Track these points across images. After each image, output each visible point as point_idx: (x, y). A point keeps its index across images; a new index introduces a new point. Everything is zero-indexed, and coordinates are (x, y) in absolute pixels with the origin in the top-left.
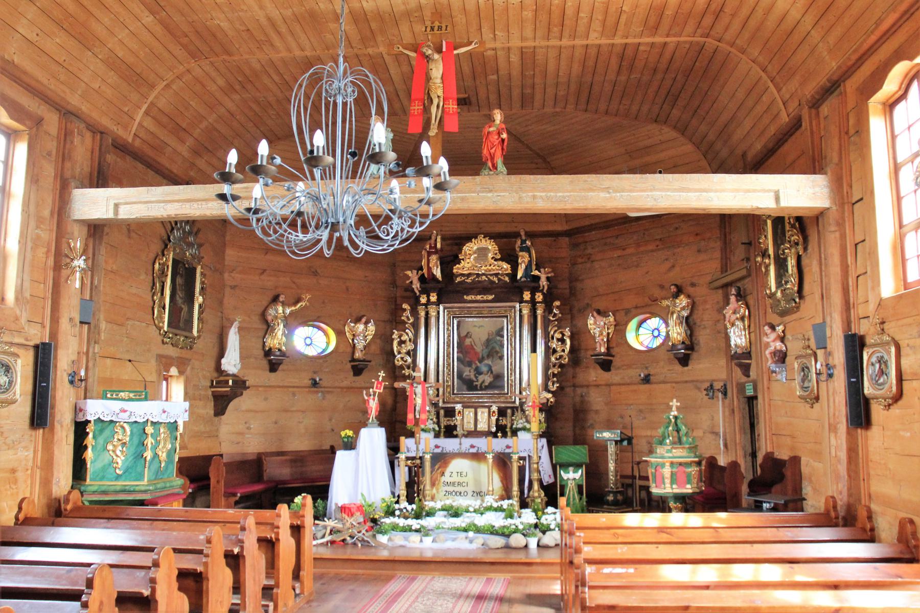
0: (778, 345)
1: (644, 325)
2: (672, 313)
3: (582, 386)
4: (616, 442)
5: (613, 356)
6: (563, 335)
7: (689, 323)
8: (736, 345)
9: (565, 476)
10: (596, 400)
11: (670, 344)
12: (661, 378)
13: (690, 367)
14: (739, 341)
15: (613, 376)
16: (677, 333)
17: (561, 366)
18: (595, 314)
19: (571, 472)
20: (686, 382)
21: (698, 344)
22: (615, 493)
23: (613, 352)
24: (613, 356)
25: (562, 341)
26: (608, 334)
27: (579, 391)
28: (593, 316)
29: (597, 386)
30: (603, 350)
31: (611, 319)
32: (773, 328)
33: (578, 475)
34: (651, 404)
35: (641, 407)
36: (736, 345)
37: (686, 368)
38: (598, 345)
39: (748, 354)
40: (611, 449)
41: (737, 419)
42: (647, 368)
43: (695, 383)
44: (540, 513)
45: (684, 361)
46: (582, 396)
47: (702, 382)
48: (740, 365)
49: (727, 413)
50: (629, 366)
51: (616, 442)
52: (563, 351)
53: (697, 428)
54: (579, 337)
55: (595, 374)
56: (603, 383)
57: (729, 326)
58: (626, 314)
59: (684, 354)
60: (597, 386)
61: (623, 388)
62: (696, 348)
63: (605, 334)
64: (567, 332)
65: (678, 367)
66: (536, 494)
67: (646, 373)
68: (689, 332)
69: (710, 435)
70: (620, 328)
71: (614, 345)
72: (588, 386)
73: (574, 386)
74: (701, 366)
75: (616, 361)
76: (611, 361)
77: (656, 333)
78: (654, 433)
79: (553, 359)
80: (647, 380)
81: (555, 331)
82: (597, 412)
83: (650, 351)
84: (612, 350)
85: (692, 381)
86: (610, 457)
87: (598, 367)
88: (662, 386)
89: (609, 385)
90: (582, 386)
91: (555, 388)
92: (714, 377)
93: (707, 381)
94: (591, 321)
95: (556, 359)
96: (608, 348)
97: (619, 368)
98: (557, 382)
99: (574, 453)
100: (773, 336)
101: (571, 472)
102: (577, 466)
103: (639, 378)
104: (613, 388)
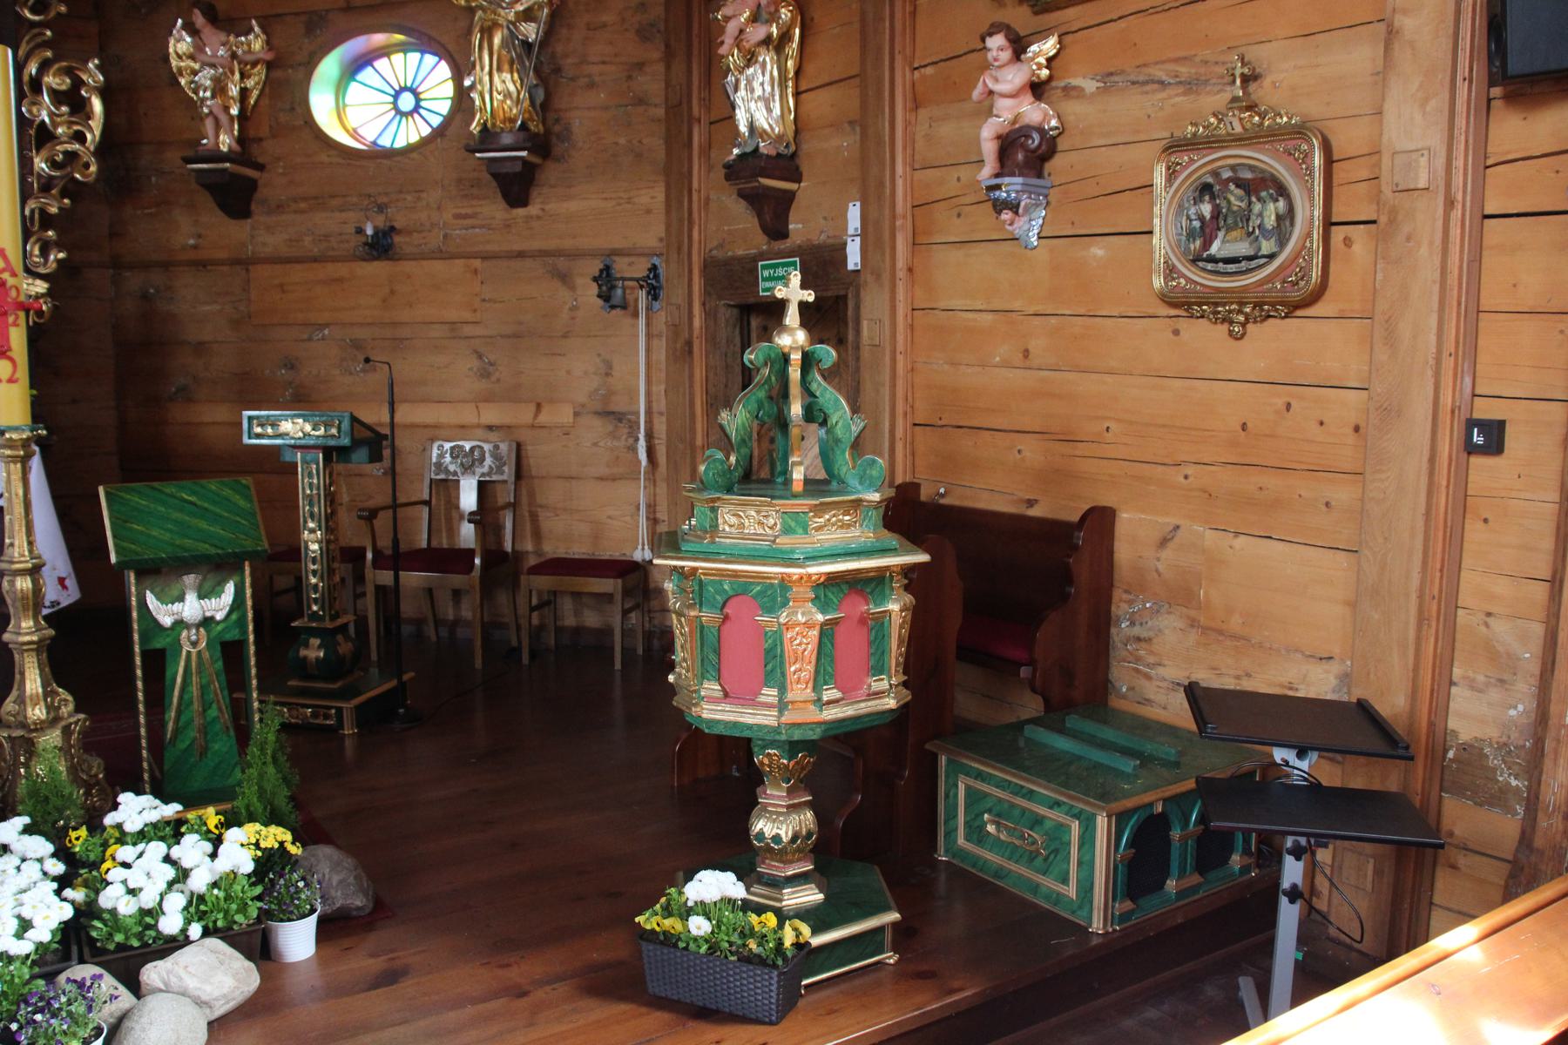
0: (1033, 112)
1: (367, 75)
2: (487, 32)
3: (146, 266)
4: (328, 452)
5: (260, 167)
6: (78, 83)
7: (541, 64)
8: (752, 127)
9: (165, 614)
10: (199, 308)
11: (475, 127)
12: (435, 240)
13: (533, 209)
14: (762, 121)
15: (262, 234)
16: (501, 90)
17: (72, 189)
18: (199, 19)
19: (191, 598)
20: (521, 255)
21: (566, 135)
22: (328, 636)
23: (261, 153)
24: (260, 167)
25: (73, 101)
26: (244, 93)
27: (134, 281)
28: (191, 28)
29: (202, 265)
30: (225, 142)
31: (257, 43)
32: (1019, 47)
33: (221, 605)
34: (394, 324)
35: (361, 334)
36: (752, 127)
37: (521, 211)
38: (209, 124)
39: (787, 164)
40: (310, 480)
41: (699, 373)
42: (381, 208)
43: (557, 262)
44: (79, 837)
45: (516, 187)
46: (145, 297)
47: (576, 255)
48: (755, 199)
49: (661, 355)
50: (318, 202)
51: (328, 452)
52: (80, 137)
53: (552, 401)
54: (140, 94)
55: (197, 228)
56: (222, 255)
57: (735, 59)
58: (310, 30)
59: (514, 163)
60: (202, 265)
61: (298, 273)
62: (558, 149)
63: (234, 91)
64: (93, 74)
65: (494, 209)
66: (38, 713)
67: (380, 221)
68: (540, 95)
69: (597, 422)
70: (286, 79)
71: (264, 131)
72: (166, 265)
73: (117, 264)
74: (573, 206)
75: (272, 186)
76: (253, 185)
77: (407, 102)
78: (853, 482)
79: (40, 164)
80: (381, 247)
81: (44, 66)
82: (200, 348)
83: (378, 155)
84: (255, 149)
85: (543, 253)
86: (304, 507)
87: (206, 200)
88: (438, 266)
89: (243, 263)
90: (146, 266)
91: (52, 265)
92: (618, 243)
93: (592, 254)
94: (180, 43)
95: (54, 164)
96: (241, 140)
97: (280, 208)
98: (60, 246)
99: (203, 513)
100: (1013, 78)
101: (191, 598)
102: (214, 567)
103: (357, 240)
104: (262, 272)
